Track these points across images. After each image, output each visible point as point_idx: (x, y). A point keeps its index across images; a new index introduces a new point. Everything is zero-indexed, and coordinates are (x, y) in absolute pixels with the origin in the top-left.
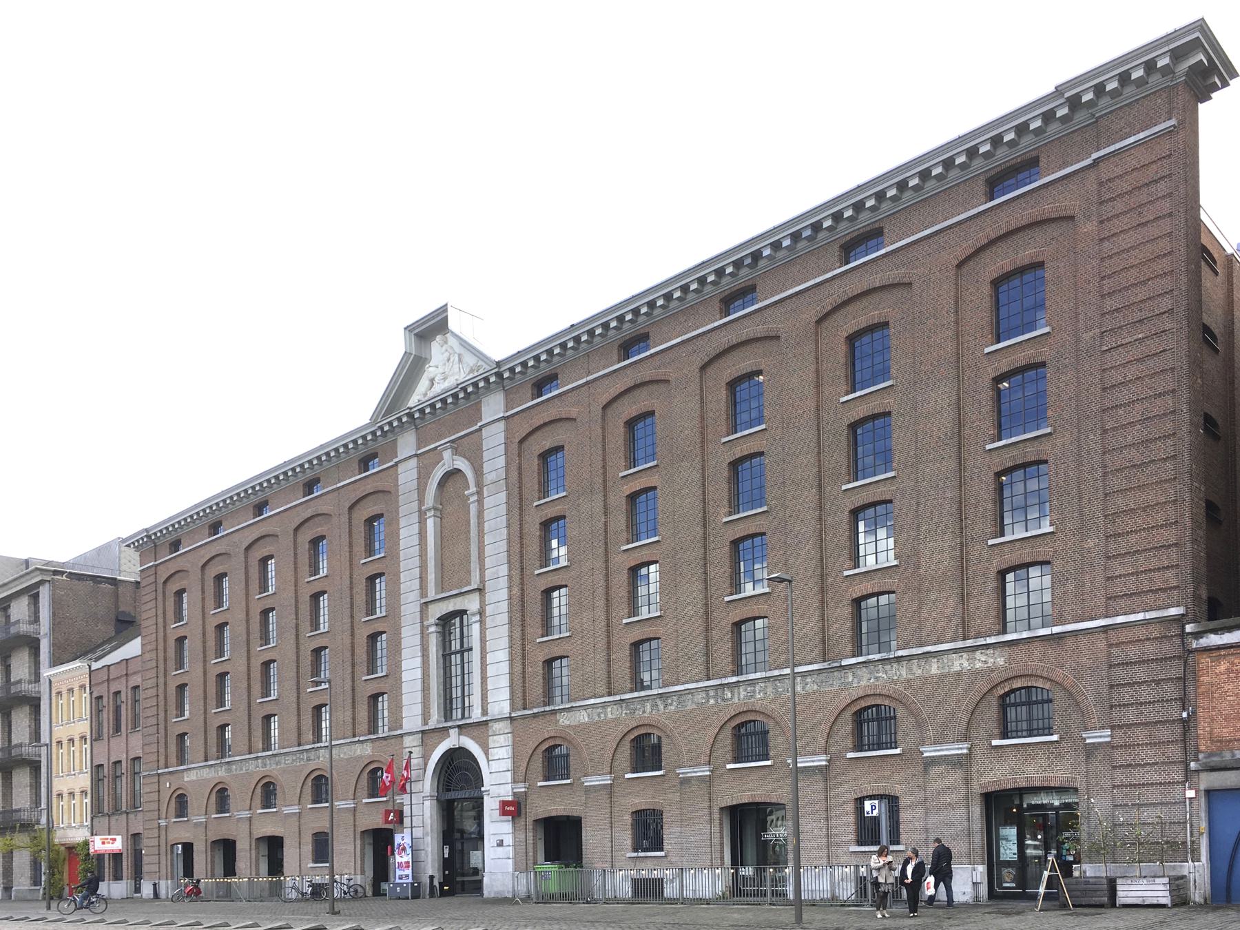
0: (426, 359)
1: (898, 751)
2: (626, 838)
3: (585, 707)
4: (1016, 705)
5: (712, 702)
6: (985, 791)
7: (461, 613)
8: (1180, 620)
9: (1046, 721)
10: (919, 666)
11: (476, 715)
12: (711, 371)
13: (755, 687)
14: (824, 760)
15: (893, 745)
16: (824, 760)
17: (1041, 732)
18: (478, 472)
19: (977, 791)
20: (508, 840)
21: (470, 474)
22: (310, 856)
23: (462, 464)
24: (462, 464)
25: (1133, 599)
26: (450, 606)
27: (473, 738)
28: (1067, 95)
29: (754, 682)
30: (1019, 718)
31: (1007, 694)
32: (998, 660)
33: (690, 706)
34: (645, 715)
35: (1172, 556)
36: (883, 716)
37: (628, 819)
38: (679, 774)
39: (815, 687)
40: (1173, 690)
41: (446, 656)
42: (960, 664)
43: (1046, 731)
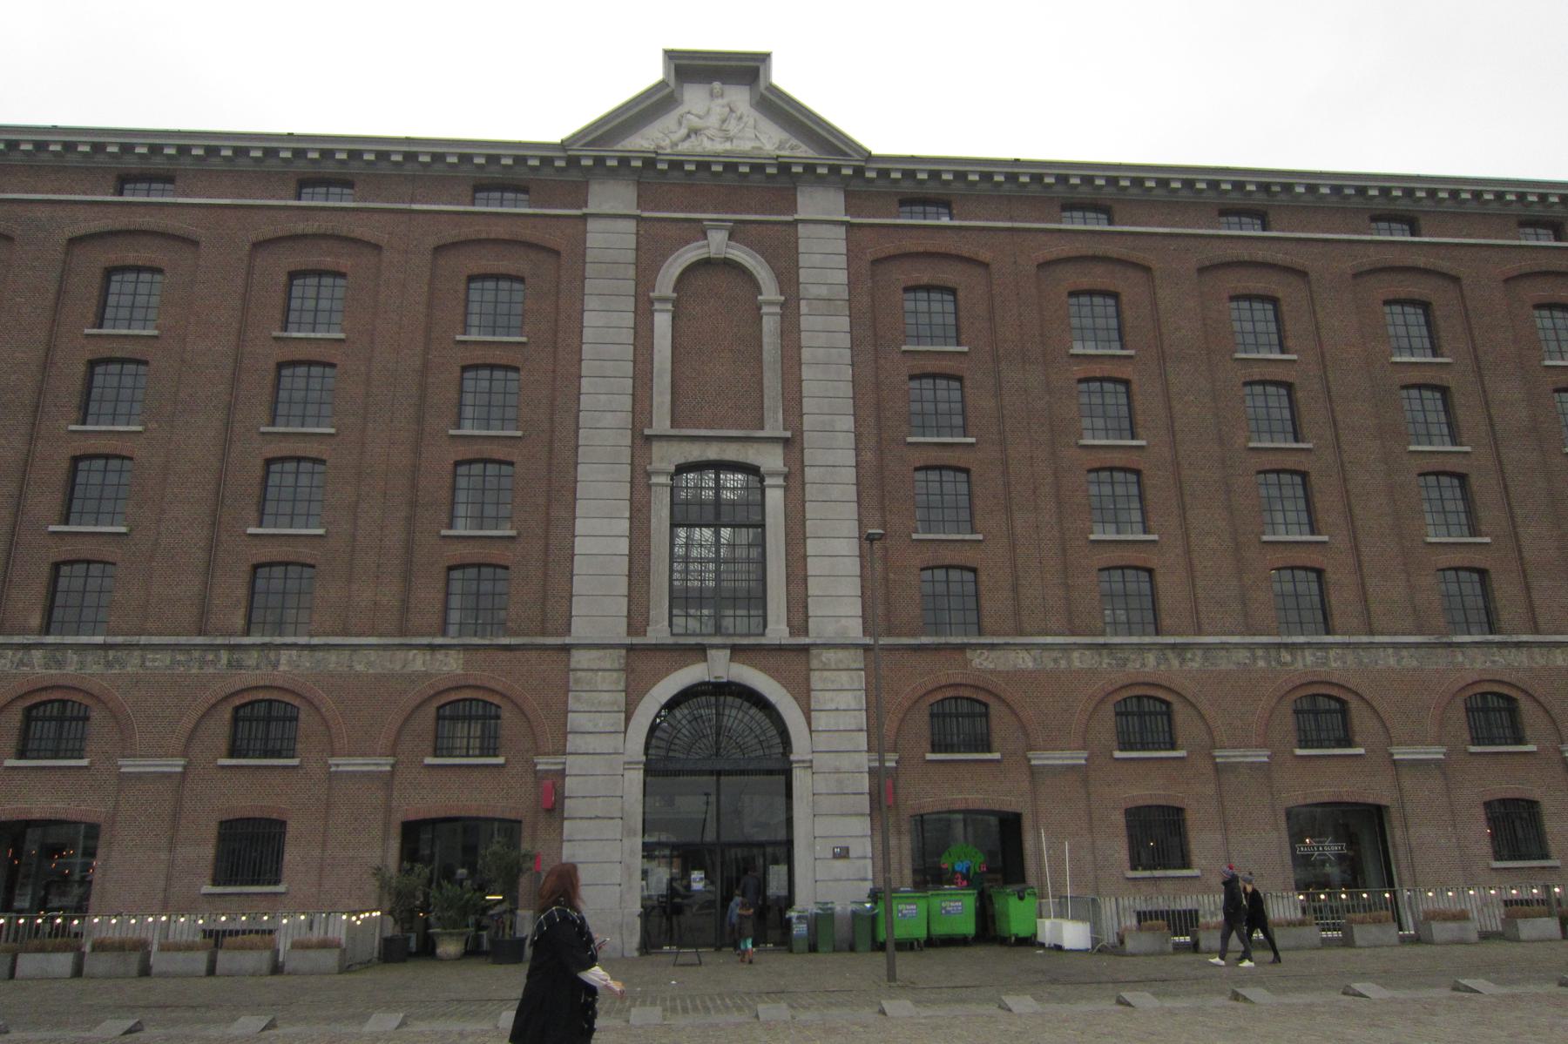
0: (676, 101)
1: (84, 762)
2: (1119, 850)
3: (1027, 647)
4: (44, 719)
5: (1261, 663)
6: (1131, 805)
9: (492, 741)
10: (1543, 655)
11: (778, 631)
13: (1327, 653)
14: (1264, 756)
15: (491, 752)
16: (386, 764)
17: (69, 754)
18: (788, 279)
19: (399, 818)
20: (863, 847)
21: (770, 291)
22: (209, 872)
27: (764, 669)
28: (570, 153)
29: (1065, 647)
30: (45, 736)
31: (36, 706)
33: (1224, 665)
34: (1146, 669)
36: (1146, 710)
37: (1119, 819)
38: (121, 766)
39: (1415, 663)
43: (76, 753)
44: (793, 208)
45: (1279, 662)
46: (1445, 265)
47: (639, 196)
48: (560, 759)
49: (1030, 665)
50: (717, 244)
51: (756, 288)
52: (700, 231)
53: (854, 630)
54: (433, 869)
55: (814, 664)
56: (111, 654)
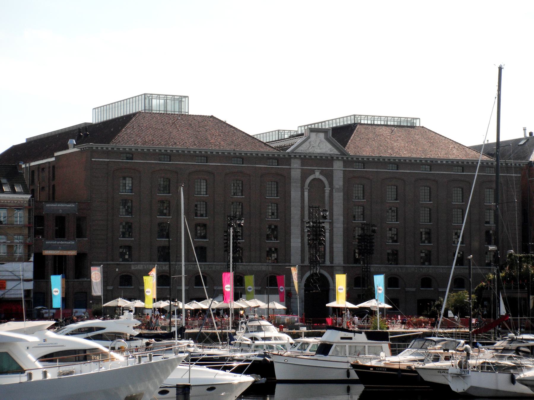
44: (290, 165)
45: (420, 271)
48: (290, 287)
49: (373, 270)
50: (317, 175)
51: (325, 187)
52: (313, 172)
53: (342, 263)
54: (481, 343)
56: (210, 266)
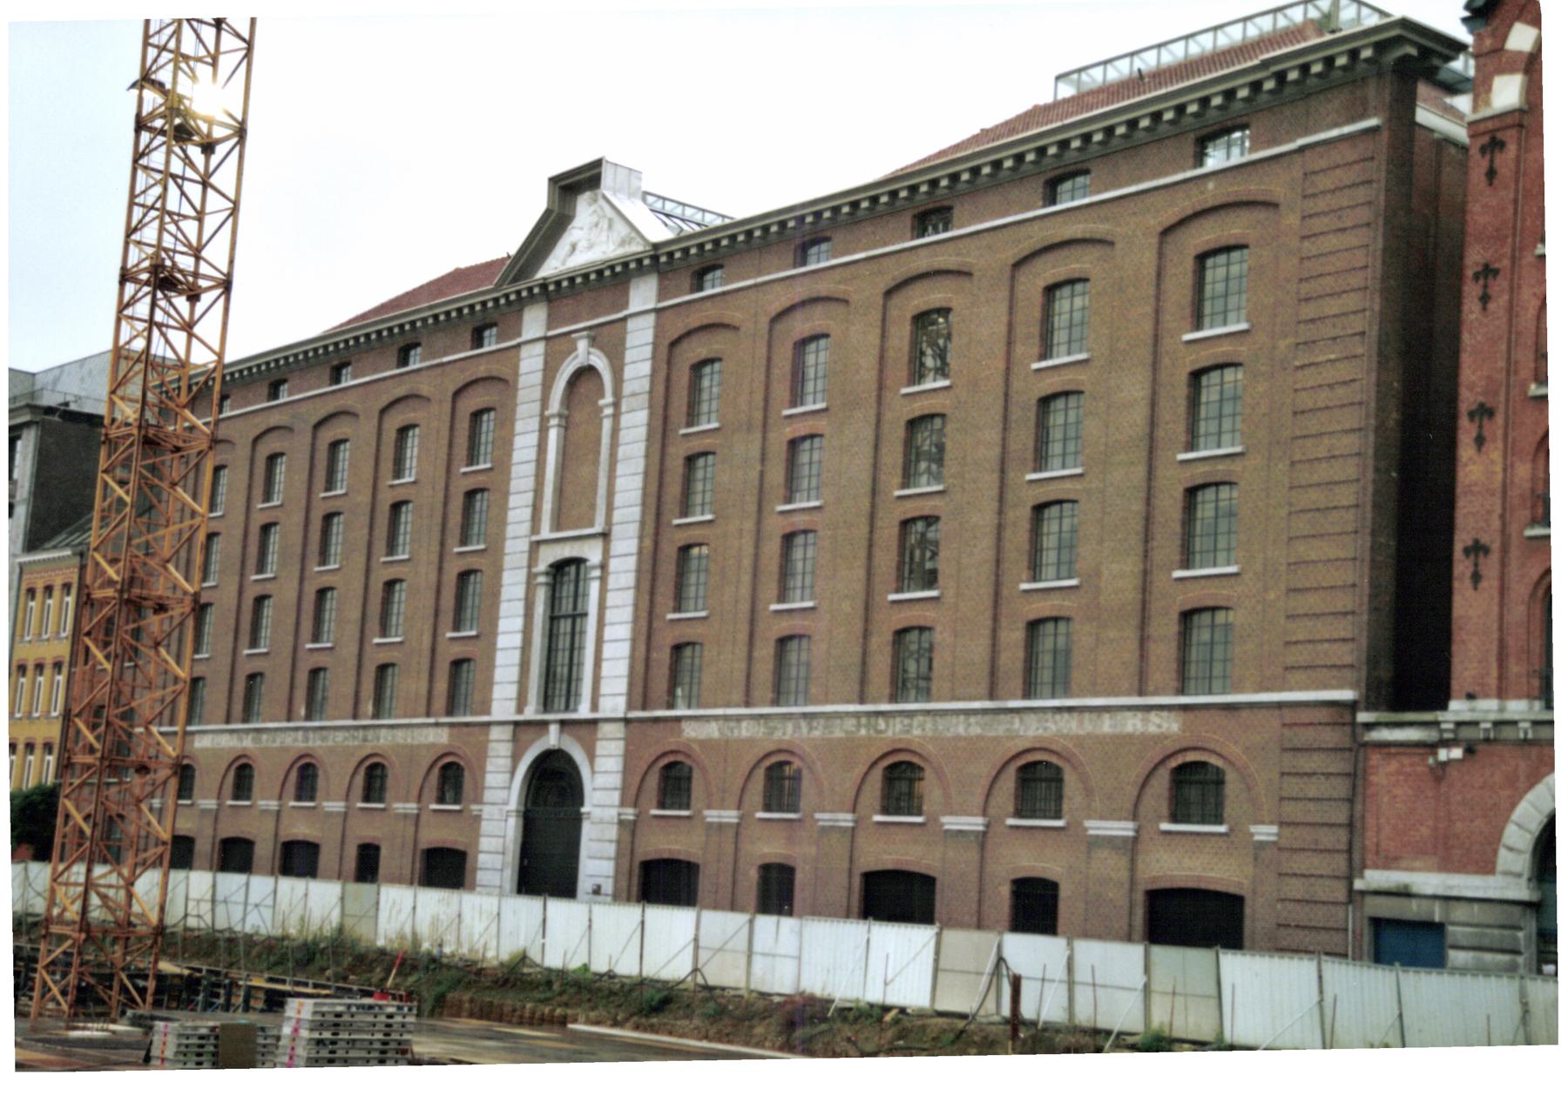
7: (578, 562)
8: (1352, 706)
11: (584, 712)
12: (897, 300)
19: (1142, 887)
23: (600, 362)
24: (600, 362)
25: (1312, 672)
26: (567, 551)
32: (1170, 725)
35: (1344, 628)
40: (1340, 788)
41: (553, 619)
42: (1132, 724)
46: (1100, 229)
47: (549, 316)
51: (602, 396)
55: (600, 735)
